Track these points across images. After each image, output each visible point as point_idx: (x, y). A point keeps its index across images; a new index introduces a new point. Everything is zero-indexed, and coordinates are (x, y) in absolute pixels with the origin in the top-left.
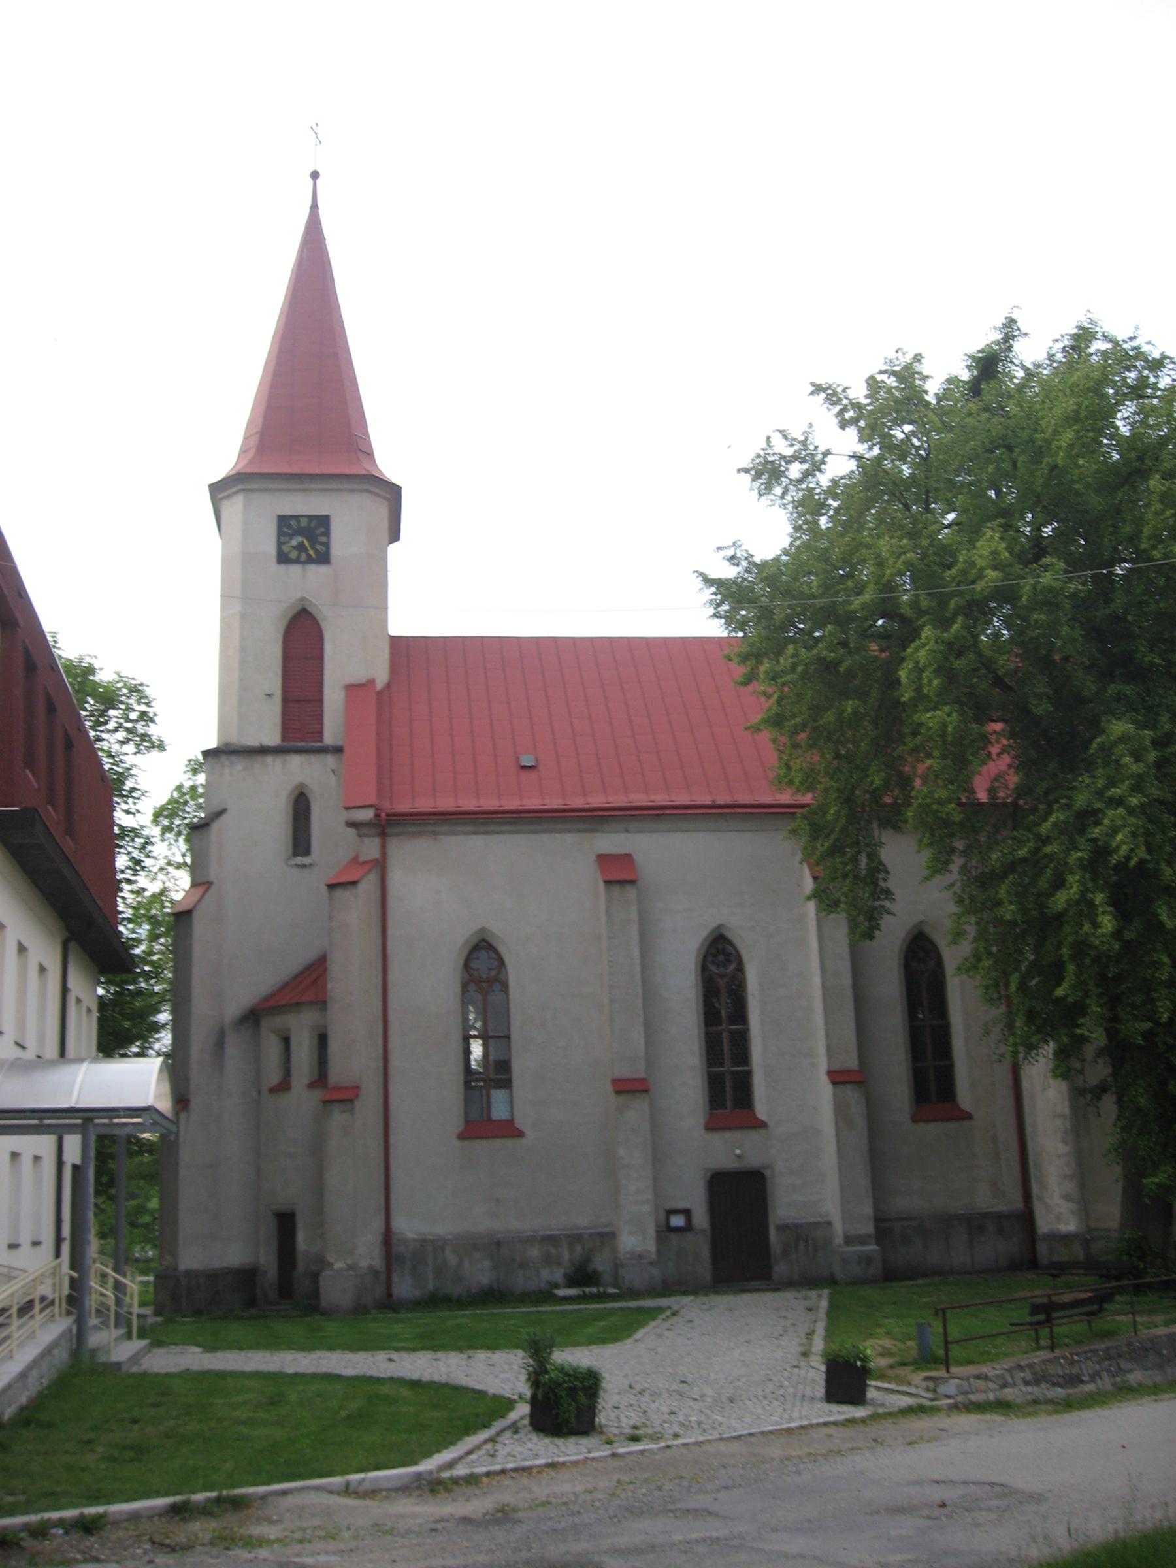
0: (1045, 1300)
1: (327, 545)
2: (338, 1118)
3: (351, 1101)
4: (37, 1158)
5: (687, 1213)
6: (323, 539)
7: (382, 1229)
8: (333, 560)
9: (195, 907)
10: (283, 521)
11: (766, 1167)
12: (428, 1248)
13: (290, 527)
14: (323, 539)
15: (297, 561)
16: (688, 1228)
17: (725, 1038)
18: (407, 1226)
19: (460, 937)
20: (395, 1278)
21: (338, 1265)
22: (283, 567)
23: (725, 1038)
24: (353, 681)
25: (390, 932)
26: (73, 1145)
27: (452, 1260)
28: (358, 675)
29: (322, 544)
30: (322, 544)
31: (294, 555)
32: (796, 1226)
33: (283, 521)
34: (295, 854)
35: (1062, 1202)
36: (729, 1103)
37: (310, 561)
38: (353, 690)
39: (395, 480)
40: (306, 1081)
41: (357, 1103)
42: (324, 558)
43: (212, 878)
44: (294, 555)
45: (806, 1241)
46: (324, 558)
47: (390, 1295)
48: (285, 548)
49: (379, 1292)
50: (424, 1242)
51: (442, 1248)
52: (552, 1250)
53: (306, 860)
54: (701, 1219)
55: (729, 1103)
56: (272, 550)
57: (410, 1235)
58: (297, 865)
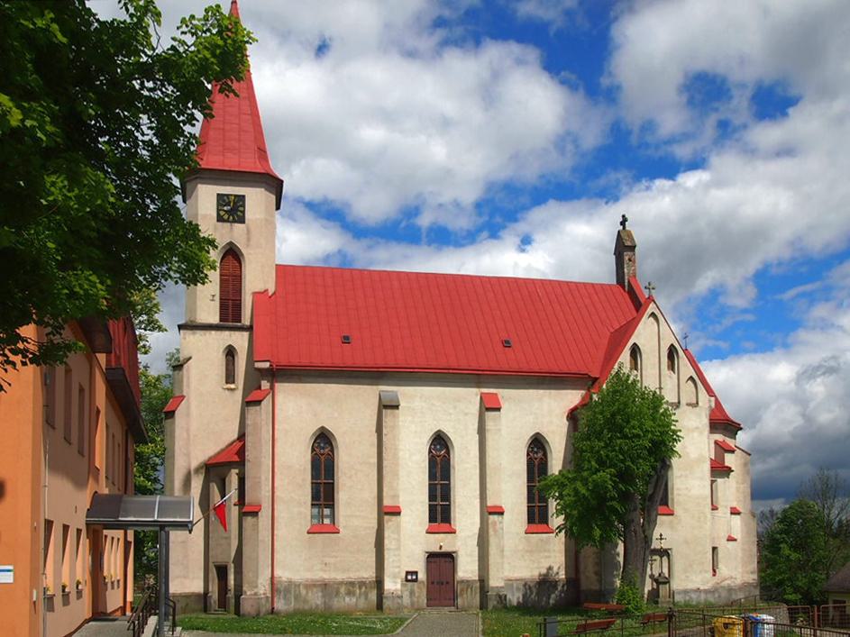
0: (584, 622)
1: (243, 212)
2: (249, 520)
3: (257, 513)
4: (118, 539)
5: (416, 573)
6: (241, 209)
7: (270, 576)
8: (246, 221)
9: (242, 437)
10: (220, 196)
11: (454, 552)
12: (291, 587)
13: (224, 201)
14: (241, 209)
15: (227, 221)
16: (416, 580)
17: (439, 508)
18: (283, 574)
19: (312, 429)
20: (276, 599)
21: (248, 593)
22: (220, 224)
23: (439, 508)
24: (257, 290)
25: (276, 427)
26: (131, 534)
27: (303, 592)
28: (260, 288)
29: (241, 211)
30: (241, 211)
31: (226, 217)
32: (468, 581)
33: (220, 196)
34: (227, 383)
35: (593, 575)
36: (537, 521)
37: (234, 221)
38: (256, 294)
39: (281, 178)
40: (404, 517)
41: (260, 513)
42: (242, 220)
43: (185, 394)
44: (226, 217)
45: (471, 589)
46: (242, 220)
47: (273, 608)
48: (222, 213)
49: (269, 606)
50: (290, 582)
51: (299, 585)
52: (351, 588)
53: (232, 386)
54: (422, 576)
55: (537, 521)
56: (215, 215)
57: (284, 579)
58: (228, 389)
